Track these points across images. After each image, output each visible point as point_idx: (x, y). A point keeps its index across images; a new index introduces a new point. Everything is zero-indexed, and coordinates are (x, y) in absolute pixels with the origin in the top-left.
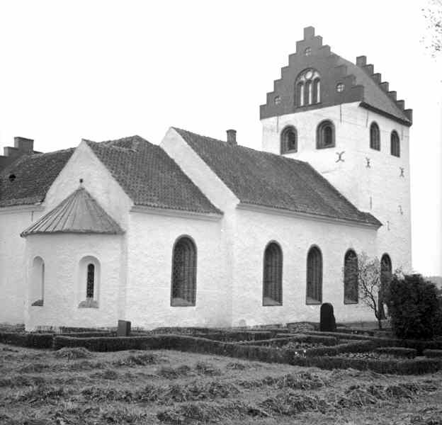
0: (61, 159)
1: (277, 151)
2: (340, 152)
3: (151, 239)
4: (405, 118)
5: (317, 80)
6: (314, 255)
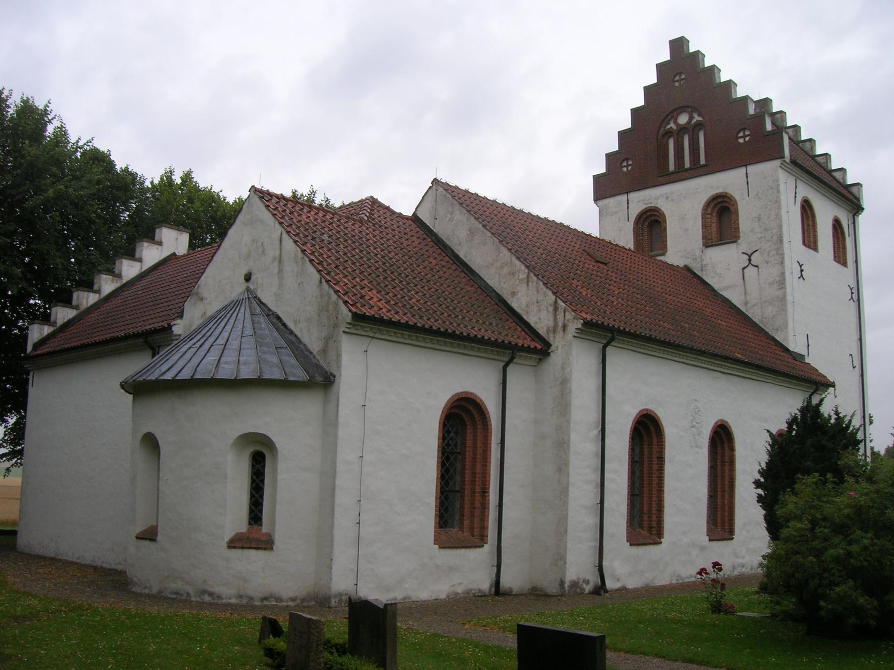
0: (240, 205)
3: (393, 400)
4: (849, 198)
5: (699, 125)
6: (721, 438)
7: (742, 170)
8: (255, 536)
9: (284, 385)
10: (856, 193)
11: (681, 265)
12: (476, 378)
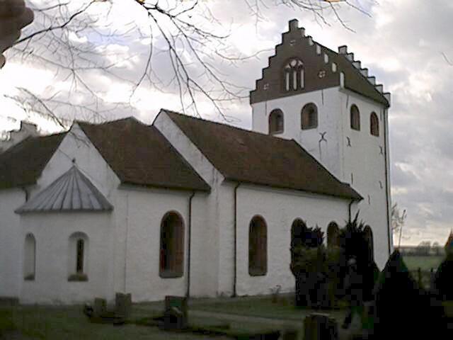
0: (56, 139)
1: (266, 132)
2: (322, 133)
4: (383, 101)
5: (301, 66)
7: (320, 92)
8: (79, 275)
9: (91, 211)
10: (387, 98)
11: (290, 139)
12: (176, 204)
